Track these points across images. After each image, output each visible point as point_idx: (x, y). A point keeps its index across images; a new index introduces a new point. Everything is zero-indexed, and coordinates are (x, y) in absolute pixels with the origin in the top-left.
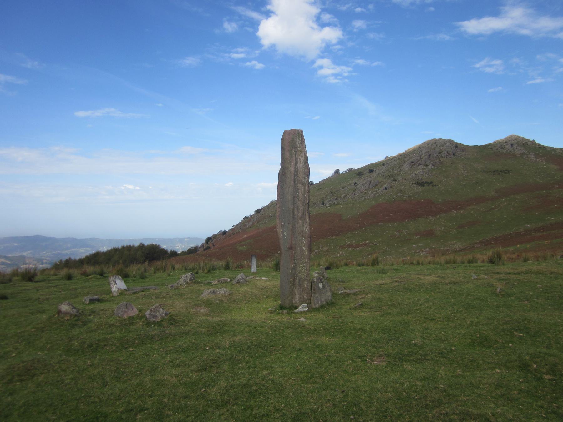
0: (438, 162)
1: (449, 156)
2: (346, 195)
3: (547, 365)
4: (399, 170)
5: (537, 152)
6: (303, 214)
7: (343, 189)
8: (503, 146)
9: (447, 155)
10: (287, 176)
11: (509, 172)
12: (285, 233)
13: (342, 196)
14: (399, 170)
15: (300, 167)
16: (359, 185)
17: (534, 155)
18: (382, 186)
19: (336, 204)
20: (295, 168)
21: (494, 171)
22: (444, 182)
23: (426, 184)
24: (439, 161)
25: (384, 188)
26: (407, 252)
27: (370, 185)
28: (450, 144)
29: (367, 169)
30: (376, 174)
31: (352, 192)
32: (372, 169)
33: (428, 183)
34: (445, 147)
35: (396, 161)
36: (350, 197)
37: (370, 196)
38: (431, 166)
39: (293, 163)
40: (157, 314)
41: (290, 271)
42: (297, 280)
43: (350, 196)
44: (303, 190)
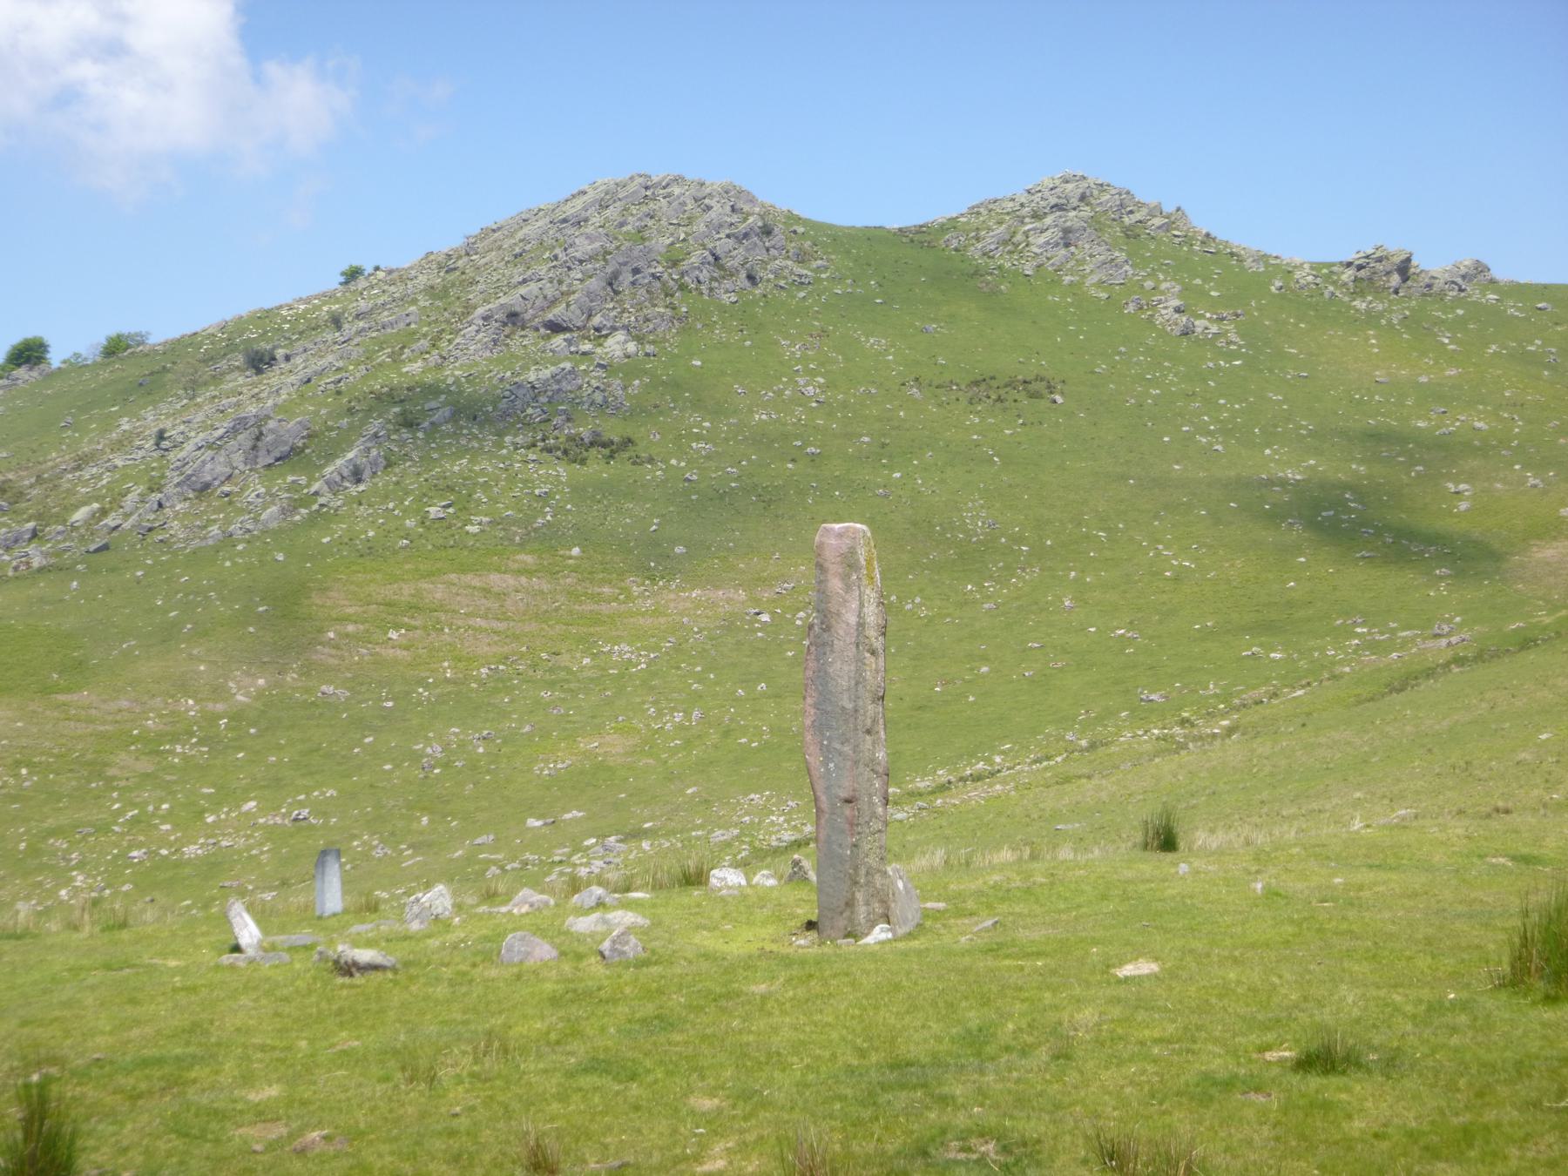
0: (662, 316)
1: (727, 284)
2: (104, 512)
3: (1394, 922)
4: (434, 358)
5: (1198, 281)
6: (875, 721)
7: (78, 468)
8: (1019, 237)
9: (713, 279)
10: (838, 634)
11: (1051, 389)
12: (831, 765)
13: (80, 515)
14: (434, 358)
15: (417, 488)
16: (189, 447)
17: (1180, 296)
18: (330, 457)
19: (36, 563)
20: (859, 616)
21: (976, 383)
22: (698, 438)
23: (593, 451)
24: (669, 312)
25: (346, 473)
26: (494, 862)
27: (254, 448)
28: (733, 209)
29: (231, 347)
30: (292, 379)
31: (141, 488)
32: (264, 346)
33: (604, 445)
34: (702, 228)
35: (414, 302)
36: (127, 525)
37: (256, 520)
38: (620, 336)
39: (855, 605)
40: (626, 948)
41: (849, 852)
42: (863, 871)
43: (127, 516)
44: (874, 666)
